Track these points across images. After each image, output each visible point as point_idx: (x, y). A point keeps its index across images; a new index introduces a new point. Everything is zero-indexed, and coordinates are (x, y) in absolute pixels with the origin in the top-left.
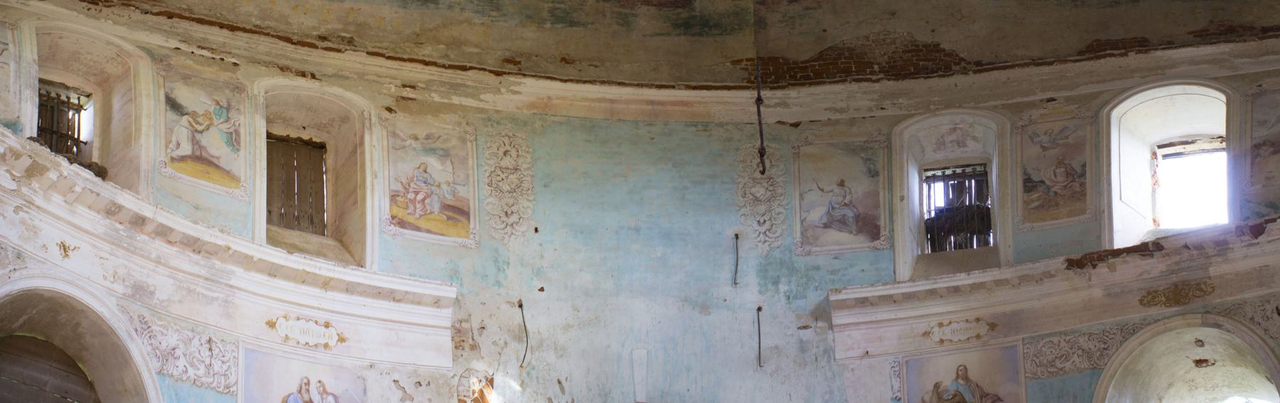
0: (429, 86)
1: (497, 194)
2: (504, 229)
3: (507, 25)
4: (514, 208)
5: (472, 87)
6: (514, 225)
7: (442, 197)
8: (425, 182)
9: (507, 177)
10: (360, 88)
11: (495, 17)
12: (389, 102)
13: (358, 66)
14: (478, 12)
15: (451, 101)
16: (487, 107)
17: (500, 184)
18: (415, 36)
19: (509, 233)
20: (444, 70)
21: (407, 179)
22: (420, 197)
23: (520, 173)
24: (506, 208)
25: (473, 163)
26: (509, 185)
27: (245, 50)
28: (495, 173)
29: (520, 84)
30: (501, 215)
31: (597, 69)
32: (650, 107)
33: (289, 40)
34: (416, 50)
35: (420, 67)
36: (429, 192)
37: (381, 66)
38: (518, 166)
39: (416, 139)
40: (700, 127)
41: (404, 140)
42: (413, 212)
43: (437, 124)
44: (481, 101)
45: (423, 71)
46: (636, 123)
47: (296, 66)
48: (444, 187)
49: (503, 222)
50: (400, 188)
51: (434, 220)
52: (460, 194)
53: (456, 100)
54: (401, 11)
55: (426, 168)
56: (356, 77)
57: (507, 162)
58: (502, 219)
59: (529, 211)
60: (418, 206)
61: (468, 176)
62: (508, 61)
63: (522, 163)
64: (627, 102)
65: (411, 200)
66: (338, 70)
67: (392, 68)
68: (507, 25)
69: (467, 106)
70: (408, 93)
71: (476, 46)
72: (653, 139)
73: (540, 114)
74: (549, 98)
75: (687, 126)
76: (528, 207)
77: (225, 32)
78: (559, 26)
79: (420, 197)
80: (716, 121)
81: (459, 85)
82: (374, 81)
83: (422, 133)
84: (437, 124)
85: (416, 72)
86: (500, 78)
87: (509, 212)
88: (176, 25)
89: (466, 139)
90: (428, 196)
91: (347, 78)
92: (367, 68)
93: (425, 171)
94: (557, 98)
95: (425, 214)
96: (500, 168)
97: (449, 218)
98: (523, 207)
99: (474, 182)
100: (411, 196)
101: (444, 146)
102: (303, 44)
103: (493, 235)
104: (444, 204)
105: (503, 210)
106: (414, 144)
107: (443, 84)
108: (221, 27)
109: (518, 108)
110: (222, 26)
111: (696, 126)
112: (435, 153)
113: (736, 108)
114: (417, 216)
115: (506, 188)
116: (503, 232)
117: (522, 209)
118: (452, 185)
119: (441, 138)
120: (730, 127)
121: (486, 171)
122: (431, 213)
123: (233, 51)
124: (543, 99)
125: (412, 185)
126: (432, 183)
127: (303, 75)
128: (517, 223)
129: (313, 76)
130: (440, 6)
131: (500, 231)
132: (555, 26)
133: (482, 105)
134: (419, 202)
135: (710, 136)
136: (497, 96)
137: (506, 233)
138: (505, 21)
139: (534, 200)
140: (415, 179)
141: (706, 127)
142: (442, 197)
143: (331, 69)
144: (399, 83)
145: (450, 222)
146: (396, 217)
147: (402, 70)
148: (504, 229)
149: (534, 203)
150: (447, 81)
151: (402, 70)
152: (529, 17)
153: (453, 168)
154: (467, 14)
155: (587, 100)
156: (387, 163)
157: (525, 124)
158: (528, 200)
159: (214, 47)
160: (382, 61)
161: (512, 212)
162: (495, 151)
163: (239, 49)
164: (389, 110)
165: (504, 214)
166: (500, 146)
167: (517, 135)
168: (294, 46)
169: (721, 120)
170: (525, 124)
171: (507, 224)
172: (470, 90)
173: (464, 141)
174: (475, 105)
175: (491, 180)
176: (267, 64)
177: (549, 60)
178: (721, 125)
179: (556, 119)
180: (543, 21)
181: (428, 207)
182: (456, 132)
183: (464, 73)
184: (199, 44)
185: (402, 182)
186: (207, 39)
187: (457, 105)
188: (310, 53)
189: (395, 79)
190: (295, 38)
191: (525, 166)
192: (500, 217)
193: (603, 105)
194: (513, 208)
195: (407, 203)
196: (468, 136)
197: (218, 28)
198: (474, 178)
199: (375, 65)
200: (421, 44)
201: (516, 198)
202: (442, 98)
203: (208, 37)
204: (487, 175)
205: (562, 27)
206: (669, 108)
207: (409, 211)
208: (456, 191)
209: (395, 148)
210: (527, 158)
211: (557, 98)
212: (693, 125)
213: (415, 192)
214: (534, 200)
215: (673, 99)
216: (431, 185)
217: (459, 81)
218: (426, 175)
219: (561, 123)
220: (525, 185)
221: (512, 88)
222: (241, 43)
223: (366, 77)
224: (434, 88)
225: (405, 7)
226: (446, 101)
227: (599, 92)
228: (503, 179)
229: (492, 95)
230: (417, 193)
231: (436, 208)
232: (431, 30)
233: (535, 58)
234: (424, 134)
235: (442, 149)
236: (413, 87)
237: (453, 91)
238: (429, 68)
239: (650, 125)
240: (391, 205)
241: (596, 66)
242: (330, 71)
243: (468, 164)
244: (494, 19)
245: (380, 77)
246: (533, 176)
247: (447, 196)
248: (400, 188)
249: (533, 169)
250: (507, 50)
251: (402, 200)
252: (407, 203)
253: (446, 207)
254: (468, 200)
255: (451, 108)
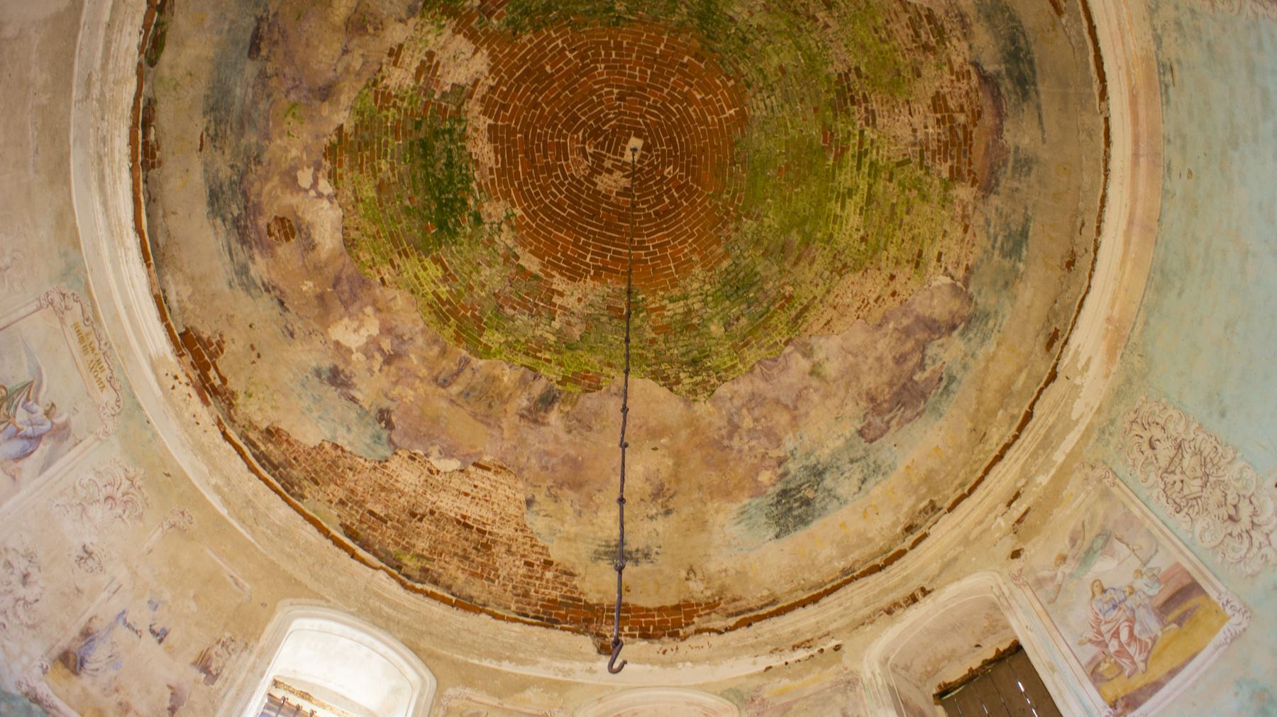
0: (1025, 473)
1: (1196, 509)
2: (1251, 544)
3: (1008, 316)
4: (1231, 499)
5: (1057, 419)
6: (1255, 520)
7: (1147, 601)
8: (1115, 607)
9: (1183, 472)
10: (973, 559)
11: (995, 325)
12: (1009, 545)
13: (957, 531)
14: (983, 341)
15: (1058, 464)
16: (1088, 421)
17: (1186, 491)
18: (973, 433)
19: (1263, 539)
20: (1019, 442)
21: (1093, 627)
22: (1124, 635)
23: (1187, 445)
24: (1224, 512)
25: (1140, 508)
26: (1195, 478)
27: (841, 616)
28: (1169, 486)
29: (1077, 353)
30: (1229, 531)
31: (1087, 224)
32: (1143, 160)
33: (876, 569)
34: (987, 448)
35: (999, 467)
36: (1128, 613)
37: (973, 509)
38: (1176, 439)
39: (1063, 559)
40: (1166, 79)
41: (1053, 578)
42: (1134, 667)
43: (1068, 512)
44: (1077, 422)
45: (1007, 466)
46: (1166, 193)
47: (900, 594)
48: (1139, 584)
49: (1240, 535)
50: (1092, 650)
51: (1165, 647)
52: (1163, 569)
53: (1059, 457)
54: (941, 422)
55: (1101, 584)
56: (962, 548)
57: (1165, 451)
58: (1235, 533)
59: (1248, 474)
60: (1132, 650)
61: (1149, 532)
62: (1049, 345)
63: (1175, 429)
64: (1134, 197)
65: (1118, 653)
66: (942, 558)
67: (983, 500)
68: (1008, 316)
69: (1073, 448)
70: (1019, 508)
71: (1020, 371)
72: (1190, 173)
73: (1125, 347)
74: (1109, 319)
75: (1168, 102)
76: (1241, 471)
77: (811, 608)
78: (1024, 253)
79: (1124, 635)
80: (1154, 48)
81: (1046, 437)
82: (981, 533)
83: (1063, 545)
84: (1068, 512)
85: (1004, 476)
86: (1060, 376)
87: (1232, 512)
88: (759, 631)
89: (1107, 487)
90: (1131, 621)
91: (956, 559)
92: (964, 525)
93: (1104, 591)
94: (1112, 307)
95: (1149, 652)
96: (1166, 471)
97: (1180, 621)
98: (1237, 480)
99: (1161, 531)
100: (1113, 646)
101: (1096, 530)
102: (889, 562)
103: (1249, 571)
104: (1158, 608)
105: (1224, 521)
106: (1066, 569)
107: (1034, 455)
108: (804, 606)
109: (1107, 376)
110: (803, 604)
111: (1167, 86)
112: (1095, 552)
113: (1125, 10)
114: (1141, 666)
115: (1194, 486)
116: (1255, 550)
117: (1239, 485)
118: (1144, 570)
119: (1086, 524)
120: (1159, 25)
121: (1158, 498)
122: (1154, 641)
123: (832, 627)
124: (1107, 330)
125: (1103, 628)
126: (1122, 597)
127: (914, 599)
128: (1255, 514)
129: (925, 592)
130: (958, 377)
131: (1251, 554)
132: (1023, 258)
133: (1082, 427)
134: (1129, 644)
135: (1179, 62)
136: (1081, 395)
137: (1260, 547)
138: (1003, 316)
139: (1235, 452)
140: (1101, 617)
141: (1167, 68)
142: (1147, 601)
143: (935, 564)
144: (1002, 507)
145: (1186, 626)
146: (1116, 700)
147: (992, 490)
148: (1251, 544)
149: (1239, 454)
150: (1034, 446)
151: (992, 490)
152: (1006, 285)
153: (1128, 545)
154: (981, 353)
155: (1123, 262)
156: (1055, 633)
157: (1129, 381)
158: (1229, 463)
159: (809, 636)
160: (967, 504)
161: (1235, 506)
162: (1141, 458)
163: (835, 621)
164: (1016, 554)
165: (1229, 522)
166: (1140, 445)
167: (1137, 406)
168: (883, 572)
169: (1150, 38)
170: (1129, 381)
171: (1247, 531)
172: (1060, 426)
173: (1106, 494)
174: (1078, 436)
175: (1175, 502)
176: (869, 620)
177: (1064, 286)
178: (1158, 40)
179: (1139, 327)
180: (1014, 269)
181: (1144, 637)
182: (1092, 493)
183: (1034, 420)
184: (792, 643)
185: (1090, 641)
186: (798, 631)
187: (1065, 461)
188: (903, 566)
189: (995, 507)
190: (879, 561)
191: (1181, 428)
192: (1230, 535)
193: (1134, 239)
194: (1230, 498)
195: (1116, 662)
196: (1105, 481)
197: (801, 608)
198: (1157, 526)
199: (967, 515)
200: (985, 434)
201: (1218, 483)
202: (1047, 471)
203: (800, 625)
204: (1163, 500)
205: (1027, 250)
206: (1143, 127)
207: (1127, 673)
208: (1155, 572)
209: (1052, 601)
210: (1171, 416)
211: (1112, 307)
212: (1166, 91)
213: (1113, 636)
214: (1235, 452)
215: (1128, 119)
216: (1124, 601)
217: (1043, 432)
218: (1108, 596)
219: (1146, 323)
220: (1207, 450)
221: (1080, 367)
222: (833, 612)
223: (972, 537)
224: (1033, 469)
225: (941, 415)
226: (1053, 471)
227: (1114, 238)
228: (1182, 481)
229: (1078, 400)
230: (1116, 634)
231: (1153, 624)
232: (978, 410)
233: (1057, 305)
234: (1067, 542)
235: (1097, 536)
236: (1017, 495)
237: (1050, 450)
238: (1007, 457)
239: (1169, 169)
240: (1099, 690)
241: (1083, 225)
242: (934, 567)
243: (1135, 517)
244: (997, 327)
245: (981, 522)
246: (1201, 426)
247: (1151, 593)
248: (1092, 650)
249: (1191, 419)
250: (1037, 336)
251: (1107, 665)
252: (1116, 662)
253: (1164, 608)
254: (1178, 565)
255: (1064, 473)
